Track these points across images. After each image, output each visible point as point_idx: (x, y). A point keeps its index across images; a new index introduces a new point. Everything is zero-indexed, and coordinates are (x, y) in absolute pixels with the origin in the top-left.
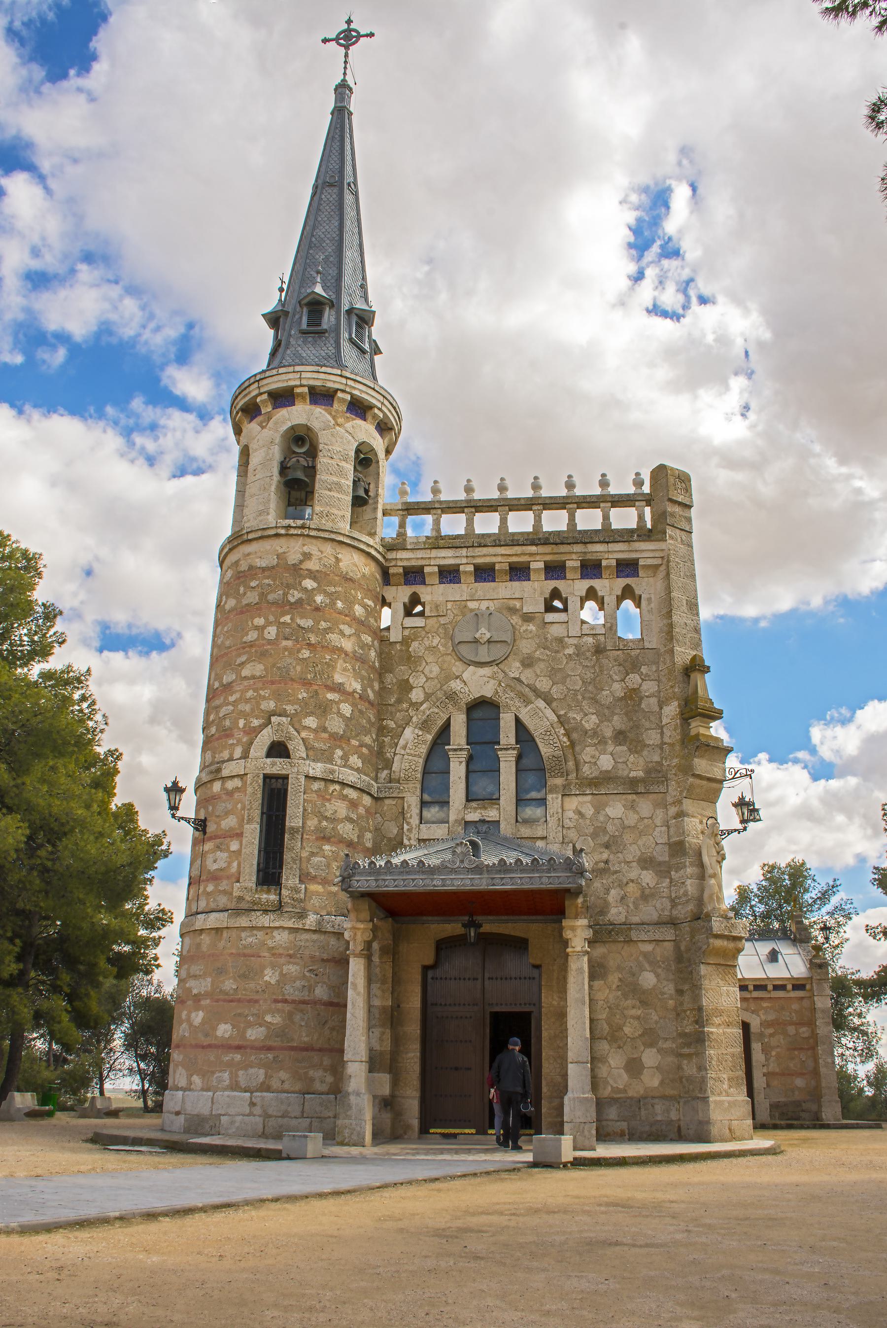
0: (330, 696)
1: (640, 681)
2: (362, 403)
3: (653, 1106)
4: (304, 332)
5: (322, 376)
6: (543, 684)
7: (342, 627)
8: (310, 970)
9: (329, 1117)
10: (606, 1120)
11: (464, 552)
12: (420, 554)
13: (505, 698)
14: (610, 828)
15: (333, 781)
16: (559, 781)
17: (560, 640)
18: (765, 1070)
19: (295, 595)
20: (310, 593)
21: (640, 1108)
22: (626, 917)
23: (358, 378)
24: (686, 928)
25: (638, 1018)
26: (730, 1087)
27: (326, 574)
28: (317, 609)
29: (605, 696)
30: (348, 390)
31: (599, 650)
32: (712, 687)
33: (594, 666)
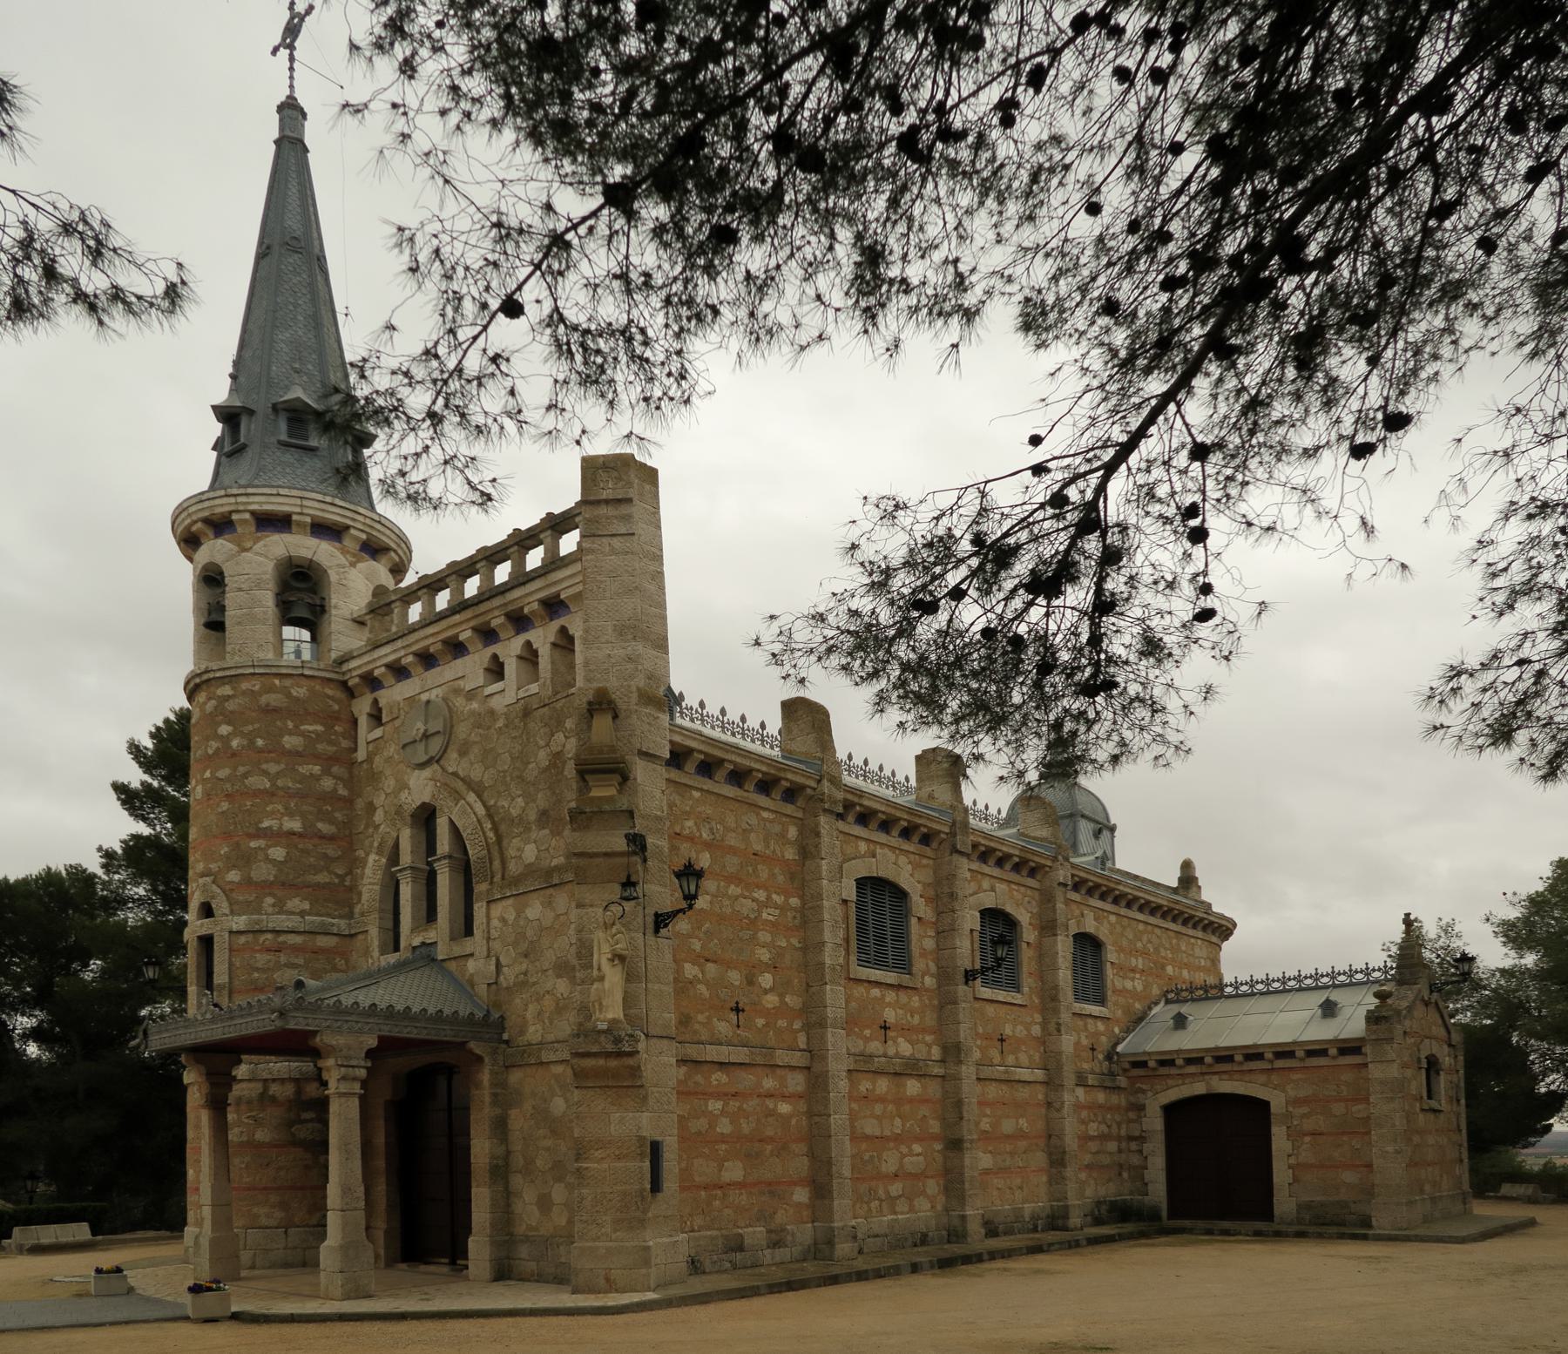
4: (280, 442)
5: (207, 504)
6: (476, 773)
11: (399, 643)
12: (366, 658)
14: (529, 933)
15: (262, 932)
18: (1292, 1161)
20: (226, 740)
23: (250, 490)
25: (548, 1149)
26: (615, 1231)
28: (234, 755)
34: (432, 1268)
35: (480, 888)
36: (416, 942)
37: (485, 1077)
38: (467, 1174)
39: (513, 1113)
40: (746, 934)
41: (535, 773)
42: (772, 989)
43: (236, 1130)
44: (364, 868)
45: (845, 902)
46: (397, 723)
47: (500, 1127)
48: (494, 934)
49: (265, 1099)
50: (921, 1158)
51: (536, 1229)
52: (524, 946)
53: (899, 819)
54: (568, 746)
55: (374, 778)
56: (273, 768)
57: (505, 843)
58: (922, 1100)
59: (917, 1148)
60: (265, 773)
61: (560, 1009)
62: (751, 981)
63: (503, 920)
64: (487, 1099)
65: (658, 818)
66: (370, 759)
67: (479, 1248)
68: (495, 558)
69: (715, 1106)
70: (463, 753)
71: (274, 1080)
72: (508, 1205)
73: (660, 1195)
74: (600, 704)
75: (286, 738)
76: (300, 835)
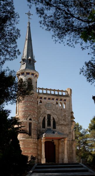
6: (56, 113)
13: (52, 114)
14: (63, 130)
16: (57, 124)
17: (57, 108)
19: (31, 100)
24: (71, 141)
29: (62, 115)
31: (61, 110)
32: (74, 115)
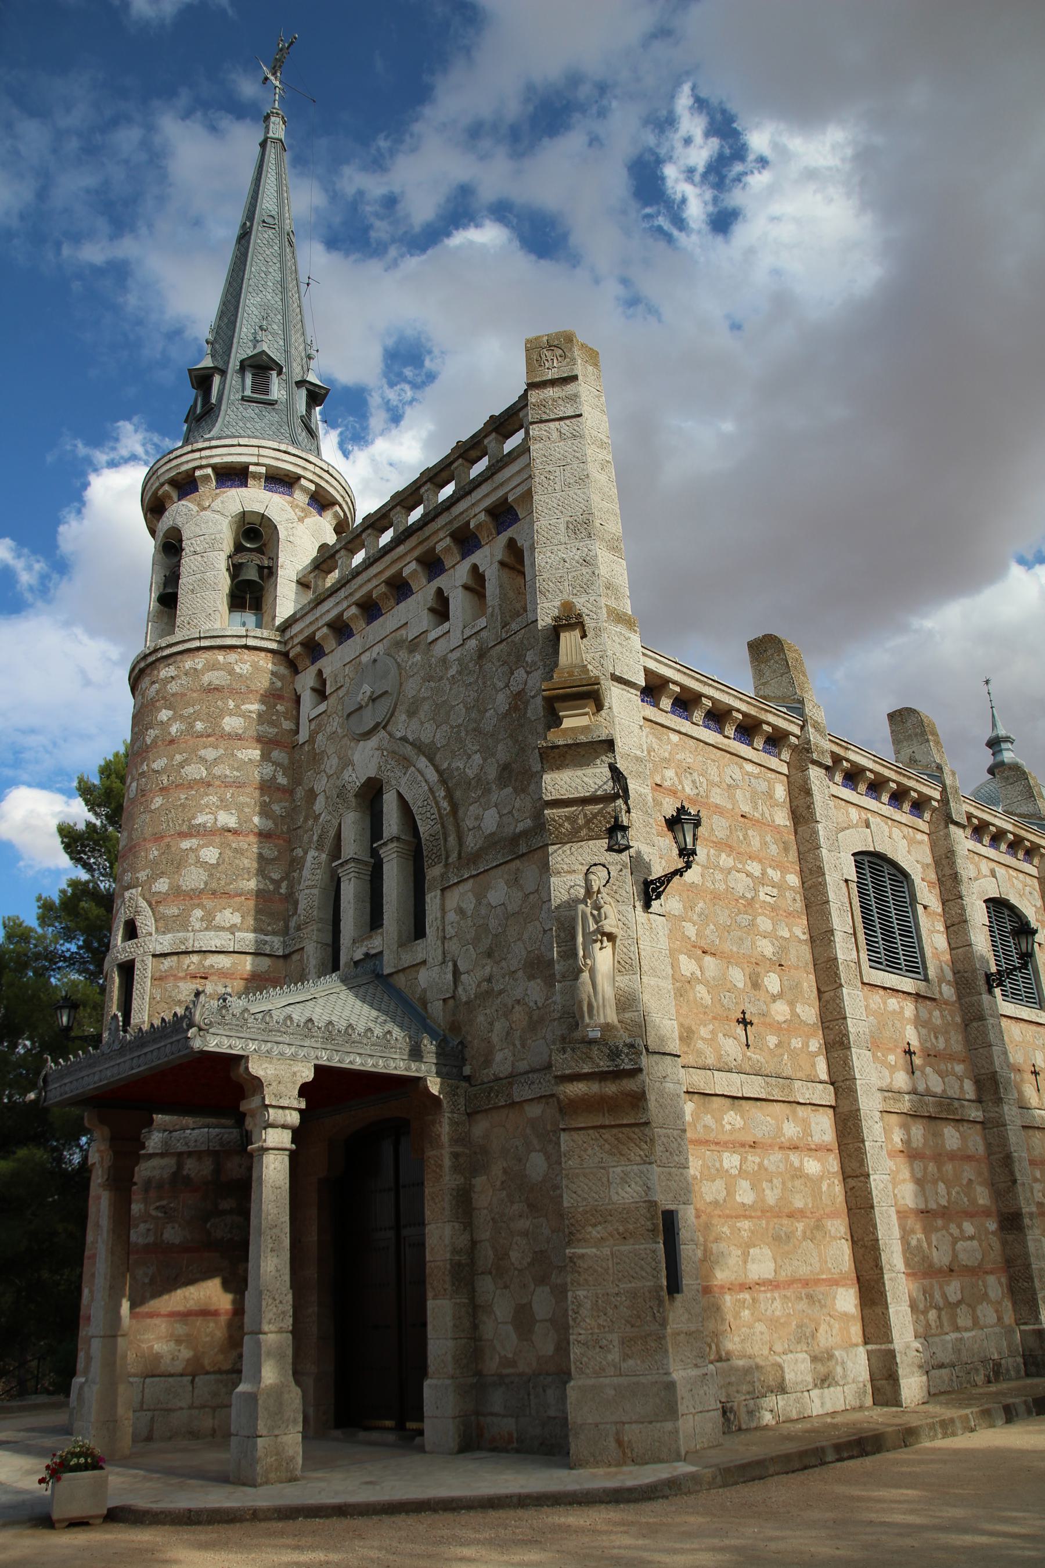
0: (186, 844)
1: (525, 676)
2: (234, 468)
3: (544, 1391)
7: (202, 752)
8: (157, 1208)
9: (181, 1408)
10: (492, 1414)
11: (342, 594)
14: (493, 923)
21: (529, 1395)
22: (513, 1064)
25: (525, 1234)
26: (625, 1357)
27: (183, 695)
30: (204, 462)
33: (476, 681)
34: (375, 1436)
35: (433, 872)
36: (358, 955)
37: (444, 1129)
38: (421, 1282)
39: (479, 1181)
40: (744, 919)
41: (494, 721)
42: (780, 996)
43: (142, 1227)
44: (301, 870)
45: (846, 881)
46: (341, 693)
47: (464, 1203)
48: (450, 931)
49: (178, 1181)
50: (975, 1243)
51: (513, 1363)
52: (486, 942)
53: (889, 780)
54: (530, 683)
55: (316, 759)
56: (210, 754)
57: (461, 813)
58: (963, 1157)
59: (969, 1228)
60: (203, 760)
61: (534, 1024)
62: (756, 984)
63: (461, 912)
64: (447, 1162)
65: (638, 759)
66: (311, 740)
67: (439, 1398)
68: (439, 480)
69: (731, 1161)
70: (411, 714)
71: (190, 1154)
72: (475, 1327)
73: (679, 1297)
74: (568, 618)
75: (227, 719)
76: (235, 832)
